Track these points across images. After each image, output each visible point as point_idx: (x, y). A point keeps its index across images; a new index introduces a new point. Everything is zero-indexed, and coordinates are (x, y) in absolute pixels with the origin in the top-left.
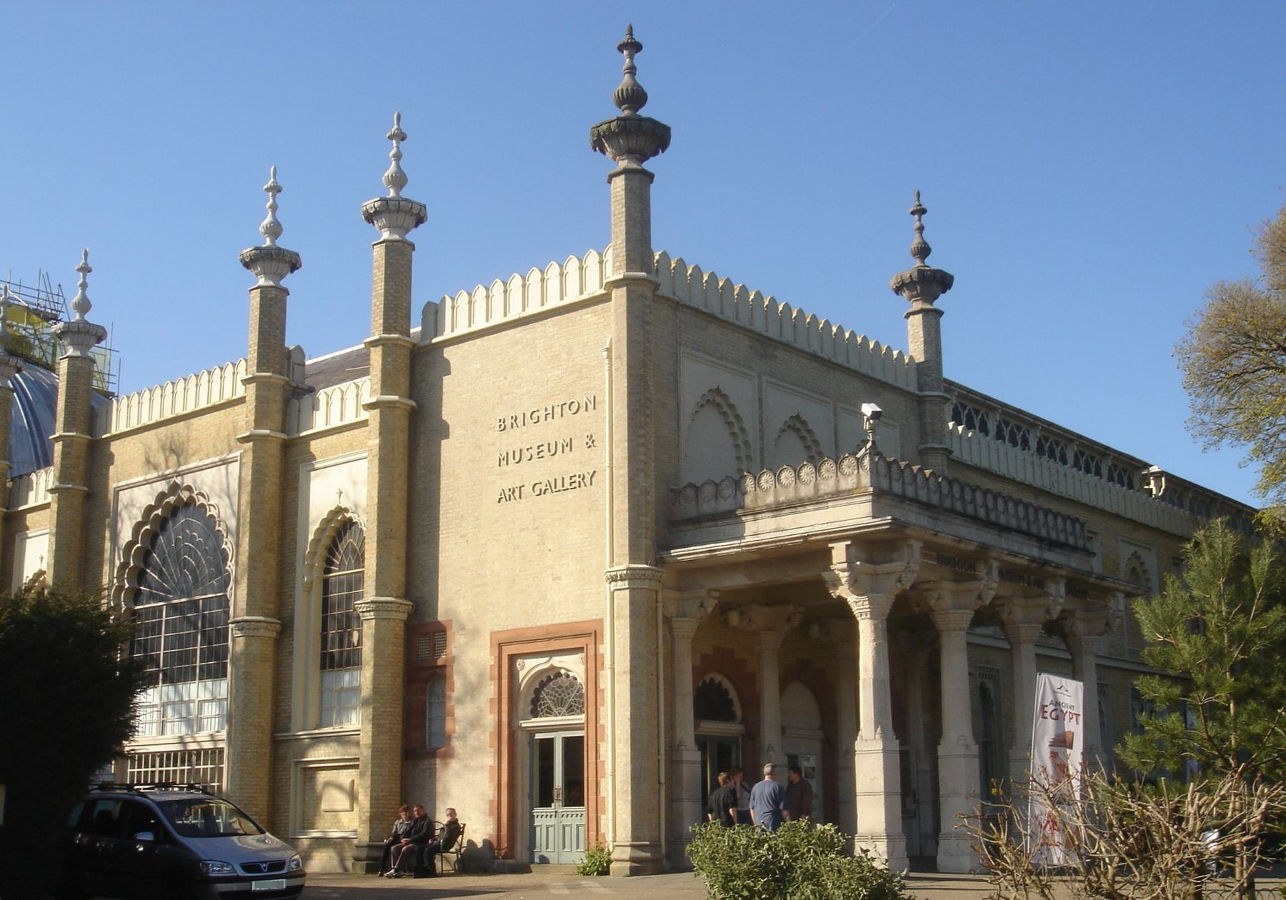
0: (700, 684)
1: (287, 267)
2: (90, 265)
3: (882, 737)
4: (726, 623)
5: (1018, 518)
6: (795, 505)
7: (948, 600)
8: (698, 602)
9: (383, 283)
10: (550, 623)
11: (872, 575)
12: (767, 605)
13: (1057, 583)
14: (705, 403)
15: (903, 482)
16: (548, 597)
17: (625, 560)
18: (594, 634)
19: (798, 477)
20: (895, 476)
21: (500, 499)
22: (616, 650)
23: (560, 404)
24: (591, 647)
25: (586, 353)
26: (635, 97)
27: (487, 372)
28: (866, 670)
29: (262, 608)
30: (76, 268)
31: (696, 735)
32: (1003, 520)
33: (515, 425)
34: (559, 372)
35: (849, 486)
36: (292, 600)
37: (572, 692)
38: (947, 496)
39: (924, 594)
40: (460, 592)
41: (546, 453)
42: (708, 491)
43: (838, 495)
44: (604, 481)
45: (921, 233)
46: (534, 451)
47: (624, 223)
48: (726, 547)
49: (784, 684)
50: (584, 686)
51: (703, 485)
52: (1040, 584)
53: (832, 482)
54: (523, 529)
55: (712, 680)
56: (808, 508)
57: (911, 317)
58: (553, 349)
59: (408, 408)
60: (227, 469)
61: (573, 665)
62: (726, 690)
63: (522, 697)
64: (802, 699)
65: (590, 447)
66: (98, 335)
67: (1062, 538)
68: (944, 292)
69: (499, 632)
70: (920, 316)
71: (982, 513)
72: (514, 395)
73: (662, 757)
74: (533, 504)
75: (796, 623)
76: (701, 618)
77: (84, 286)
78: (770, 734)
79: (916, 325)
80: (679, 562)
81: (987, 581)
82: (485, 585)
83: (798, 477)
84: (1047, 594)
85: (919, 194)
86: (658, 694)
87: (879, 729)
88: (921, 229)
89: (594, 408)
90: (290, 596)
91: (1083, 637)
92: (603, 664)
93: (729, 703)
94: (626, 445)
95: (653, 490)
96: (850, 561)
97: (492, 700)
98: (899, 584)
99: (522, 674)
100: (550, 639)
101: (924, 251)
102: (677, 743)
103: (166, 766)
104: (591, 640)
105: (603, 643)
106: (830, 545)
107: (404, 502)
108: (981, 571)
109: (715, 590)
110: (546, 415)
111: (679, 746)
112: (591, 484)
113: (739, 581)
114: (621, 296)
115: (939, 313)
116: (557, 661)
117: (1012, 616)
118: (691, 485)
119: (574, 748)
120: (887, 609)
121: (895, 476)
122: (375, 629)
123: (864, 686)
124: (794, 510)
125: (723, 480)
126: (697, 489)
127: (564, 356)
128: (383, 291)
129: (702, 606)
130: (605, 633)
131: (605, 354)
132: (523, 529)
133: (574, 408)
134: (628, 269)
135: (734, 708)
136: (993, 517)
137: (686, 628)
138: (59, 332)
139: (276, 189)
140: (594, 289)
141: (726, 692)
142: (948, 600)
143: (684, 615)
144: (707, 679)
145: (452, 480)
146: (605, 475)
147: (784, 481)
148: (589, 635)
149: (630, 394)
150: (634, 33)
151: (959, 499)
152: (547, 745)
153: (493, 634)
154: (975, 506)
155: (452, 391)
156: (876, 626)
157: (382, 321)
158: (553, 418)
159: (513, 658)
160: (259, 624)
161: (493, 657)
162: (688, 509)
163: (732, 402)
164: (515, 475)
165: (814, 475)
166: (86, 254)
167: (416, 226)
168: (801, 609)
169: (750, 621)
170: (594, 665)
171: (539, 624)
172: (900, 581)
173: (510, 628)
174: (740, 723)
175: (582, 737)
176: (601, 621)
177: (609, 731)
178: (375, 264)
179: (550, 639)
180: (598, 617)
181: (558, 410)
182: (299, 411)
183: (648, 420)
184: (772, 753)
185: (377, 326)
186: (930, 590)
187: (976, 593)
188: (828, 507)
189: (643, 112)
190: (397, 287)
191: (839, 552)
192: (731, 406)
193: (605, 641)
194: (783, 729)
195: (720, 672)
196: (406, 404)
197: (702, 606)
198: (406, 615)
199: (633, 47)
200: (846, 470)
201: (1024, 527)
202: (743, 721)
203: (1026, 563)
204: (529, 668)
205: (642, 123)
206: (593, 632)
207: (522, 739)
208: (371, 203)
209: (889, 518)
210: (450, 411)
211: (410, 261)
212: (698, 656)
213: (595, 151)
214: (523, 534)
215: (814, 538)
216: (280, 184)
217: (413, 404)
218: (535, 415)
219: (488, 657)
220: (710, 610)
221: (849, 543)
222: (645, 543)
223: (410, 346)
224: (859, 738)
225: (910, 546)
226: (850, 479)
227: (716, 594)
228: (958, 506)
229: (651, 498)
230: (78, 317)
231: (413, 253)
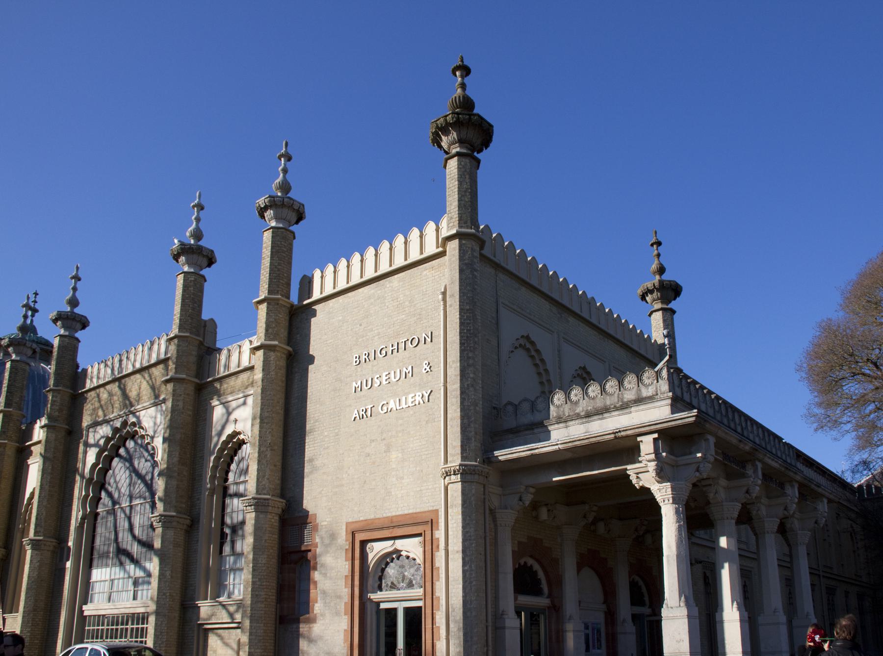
0: (517, 566)
2: (80, 276)
3: (686, 605)
4: (536, 518)
6: (601, 412)
7: (722, 495)
9: (269, 259)
10: (394, 514)
11: (673, 466)
12: (568, 505)
14: (518, 346)
15: (690, 394)
16: (393, 493)
17: (458, 459)
18: (432, 524)
19: (603, 390)
20: (685, 389)
21: (355, 418)
22: (450, 533)
23: (403, 341)
24: (428, 533)
25: (425, 299)
26: (74, 302)
27: (347, 322)
28: (669, 547)
29: (175, 507)
30: (70, 276)
31: (515, 607)
33: (367, 360)
34: (403, 316)
36: (199, 502)
39: (704, 489)
40: (323, 492)
42: (526, 406)
43: (640, 401)
44: (439, 398)
45: (658, 258)
47: (457, 193)
48: (543, 448)
50: (422, 566)
51: (519, 403)
52: (782, 486)
53: (634, 392)
54: (373, 441)
55: (525, 563)
57: (654, 313)
58: (399, 300)
59: (286, 352)
62: (536, 571)
63: (371, 575)
64: (590, 577)
65: (428, 371)
66: (84, 324)
69: (353, 522)
70: (661, 312)
72: (368, 337)
73: (490, 624)
74: (381, 421)
77: (75, 289)
78: (570, 606)
79: (657, 319)
80: (500, 461)
81: (754, 479)
82: (342, 485)
83: (603, 390)
84: (784, 494)
85: (656, 233)
86: (486, 570)
87: (683, 598)
88: (659, 255)
89: (431, 341)
90: (198, 499)
91: (799, 532)
92: (438, 547)
93: (539, 582)
94: (458, 364)
95: (481, 403)
96: (657, 452)
97: (346, 576)
98: (697, 474)
99: (370, 556)
100: (394, 527)
101: (661, 270)
102: (500, 612)
103: (139, 628)
104: (428, 528)
105: (438, 529)
106: (639, 439)
107: (281, 423)
108: (750, 472)
110: (392, 350)
111: (502, 615)
112: (428, 401)
114: (454, 249)
115: (673, 312)
116: (400, 544)
117: (759, 512)
118: (510, 403)
119: (414, 617)
120: (685, 496)
121: (685, 389)
122: (255, 520)
123: (668, 561)
124: (601, 417)
125: (537, 398)
126: (516, 407)
127: (407, 303)
128: (269, 264)
129: (520, 500)
130: (440, 521)
131: (440, 297)
132: (373, 441)
133: (415, 342)
134: (460, 227)
135: (542, 586)
137: (508, 518)
138: (54, 318)
139: (200, 207)
140: (431, 249)
142: (722, 495)
143: (506, 508)
144: (522, 562)
145: (318, 406)
146: (440, 394)
147: (591, 394)
149: (462, 324)
150: (464, 61)
152: (392, 613)
154: (735, 424)
155: (320, 339)
156: (677, 512)
157: (267, 286)
158: (398, 352)
159: (364, 543)
160: (172, 518)
161: (348, 543)
162: (509, 422)
165: (617, 387)
166: (78, 268)
169: (554, 517)
170: (430, 548)
171: (385, 515)
172: (698, 470)
173: (362, 519)
174: (547, 598)
175: (421, 607)
176: (437, 511)
177: (443, 602)
178: (264, 245)
179: (394, 527)
180: (434, 508)
181: (402, 346)
182: (210, 363)
183: (476, 346)
185: (264, 290)
186: (710, 485)
187: (745, 489)
188: (631, 412)
190: (280, 262)
191: (647, 444)
192: (537, 351)
193: (440, 528)
194: (580, 602)
195: (531, 556)
196: (285, 349)
197: (520, 500)
198: (280, 510)
199: (466, 70)
200: (646, 381)
203: (778, 466)
204: (376, 550)
205: (472, 117)
206: (430, 521)
207: (369, 607)
208: (262, 201)
209: (696, 411)
210: (314, 349)
212: (516, 542)
213: (434, 145)
214: (373, 444)
215: (623, 434)
216: (203, 203)
217: (290, 349)
218: (384, 352)
219: (344, 542)
220: (527, 503)
221: (656, 435)
222: (474, 444)
223: (289, 306)
224: (664, 605)
225: (707, 440)
226: (650, 388)
227: (532, 490)
229: (479, 408)
230: (69, 309)
231: (294, 241)
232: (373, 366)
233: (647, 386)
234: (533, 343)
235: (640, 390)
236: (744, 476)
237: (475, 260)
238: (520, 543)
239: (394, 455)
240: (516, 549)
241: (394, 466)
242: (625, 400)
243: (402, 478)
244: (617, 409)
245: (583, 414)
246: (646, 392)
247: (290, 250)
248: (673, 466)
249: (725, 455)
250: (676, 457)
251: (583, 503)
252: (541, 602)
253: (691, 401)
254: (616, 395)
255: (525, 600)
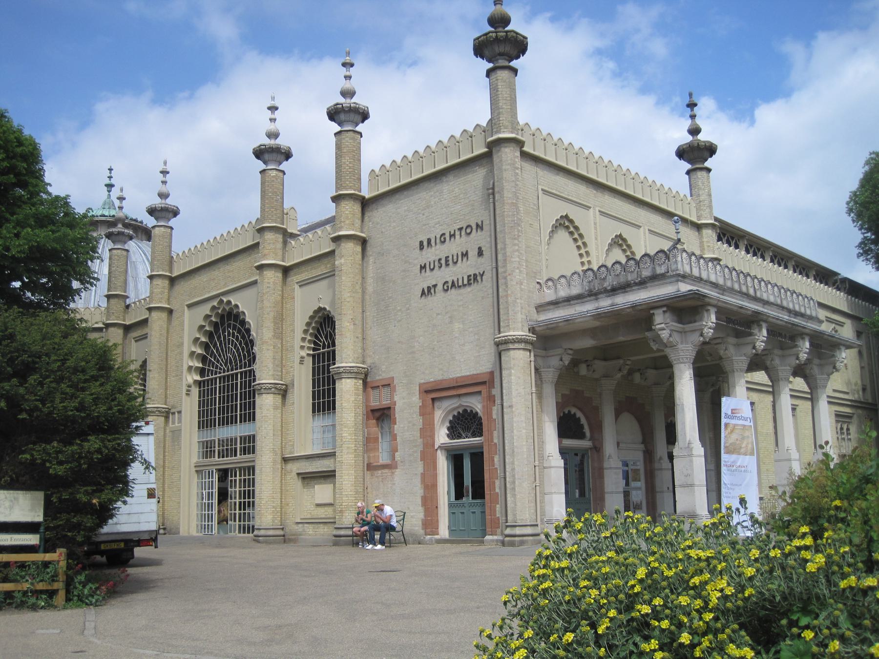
1: (283, 157)
5: (775, 296)
8: (559, 357)
13: (803, 339)
32: (765, 297)
35: (663, 271)
37: (475, 422)
38: (728, 279)
41: (450, 262)
46: (443, 262)
49: (618, 413)
52: (793, 338)
53: (650, 269)
55: (569, 412)
56: (634, 288)
60: (560, 467)
61: (476, 405)
62: (579, 418)
64: (629, 422)
67: (803, 310)
68: (711, 156)
71: (751, 292)
75: (625, 372)
76: (561, 369)
78: (609, 447)
93: (582, 427)
105: (494, 388)
106: (652, 312)
109: (571, 349)
113: (588, 343)
119: (478, 457)
129: (561, 360)
136: (758, 295)
141: (579, 419)
148: (484, 383)
151: (736, 282)
153: (420, 385)
154: (747, 287)
163: (576, 224)
164: (430, 278)
167: (363, 122)
168: (629, 362)
169: (594, 371)
171: (451, 377)
174: (590, 440)
181: (457, 233)
184: (611, 460)
189: (702, 137)
194: (618, 444)
195: (574, 406)
201: (779, 302)
202: (592, 439)
211: (360, 143)
220: (567, 363)
221: (665, 309)
227: (570, 352)
228: (736, 287)
232: (436, 250)
233: (660, 265)
234: (571, 221)
235: (655, 268)
236: (751, 334)
237: (517, 160)
238: (563, 395)
239: (457, 326)
240: (560, 401)
241: (457, 335)
242: (643, 276)
243: (463, 345)
244: (636, 284)
245: (609, 288)
246: (660, 270)
247: (359, 149)
248: (681, 332)
249: (729, 320)
250: (683, 324)
251: (618, 358)
252: (585, 444)
253: (700, 274)
254: (636, 272)
255: (568, 442)
